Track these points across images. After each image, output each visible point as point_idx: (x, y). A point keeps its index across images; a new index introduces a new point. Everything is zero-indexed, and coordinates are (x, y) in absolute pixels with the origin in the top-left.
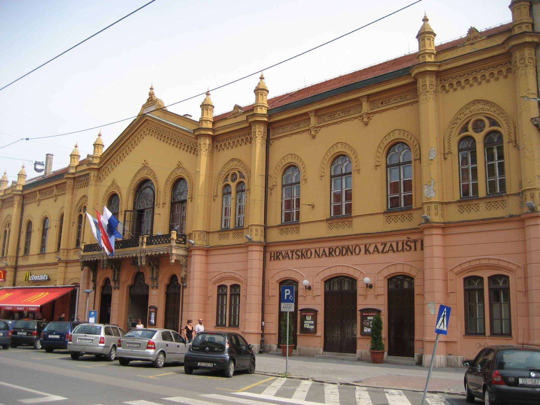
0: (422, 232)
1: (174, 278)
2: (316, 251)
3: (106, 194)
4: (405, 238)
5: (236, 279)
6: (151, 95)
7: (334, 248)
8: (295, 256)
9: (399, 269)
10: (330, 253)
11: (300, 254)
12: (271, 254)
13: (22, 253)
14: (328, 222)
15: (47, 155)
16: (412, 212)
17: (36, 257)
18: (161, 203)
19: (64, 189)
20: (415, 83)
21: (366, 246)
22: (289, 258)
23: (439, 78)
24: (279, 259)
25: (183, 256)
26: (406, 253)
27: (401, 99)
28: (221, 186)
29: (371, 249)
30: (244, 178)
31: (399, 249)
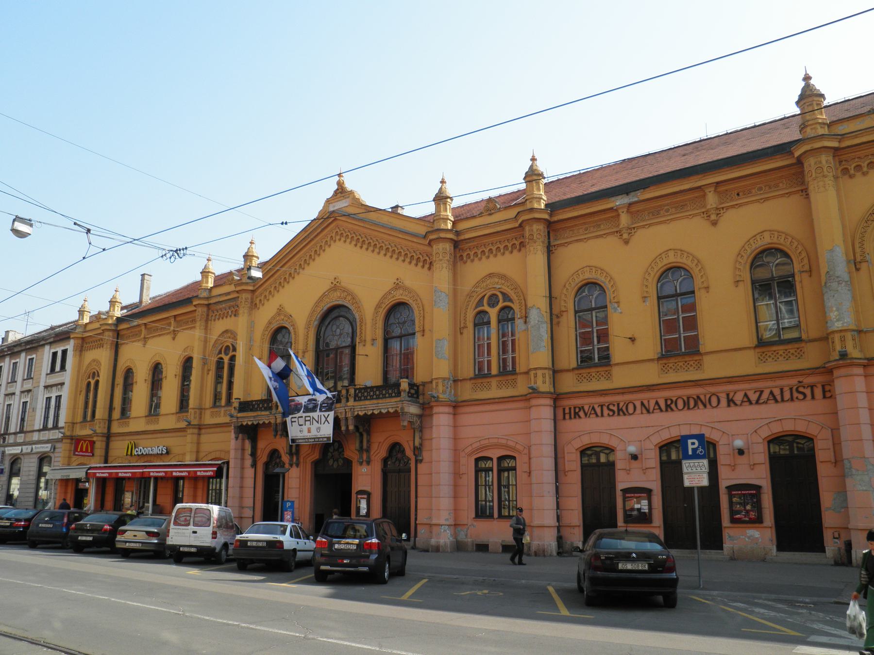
0: (830, 372)
1: (395, 449)
2: (642, 404)
3: (265, 330)
4: (793, 382)
5: (506, 447)
6: (340, 185)
7: (674, 399)
8: (606, 412)
9: (789, 427)
10: (668, 406)
11: (615, 409)
12: (564, 409)
13: (116, 414)
14: (661, 362)
15: (143, 275)
16: (803, 345)
17: (143, 420)
18: (369, 338)
19: (194, 321)
20: (800, 162)
21: (728, 395)
22: (597, 416)
23: (837, 158)
24: (580, 417)
25: (417, 415)
26: (796, 404)
27: (770, 188)
28: (471, 315)
29: (739, 397)
30: (511, 300)
31: (786, 398)
